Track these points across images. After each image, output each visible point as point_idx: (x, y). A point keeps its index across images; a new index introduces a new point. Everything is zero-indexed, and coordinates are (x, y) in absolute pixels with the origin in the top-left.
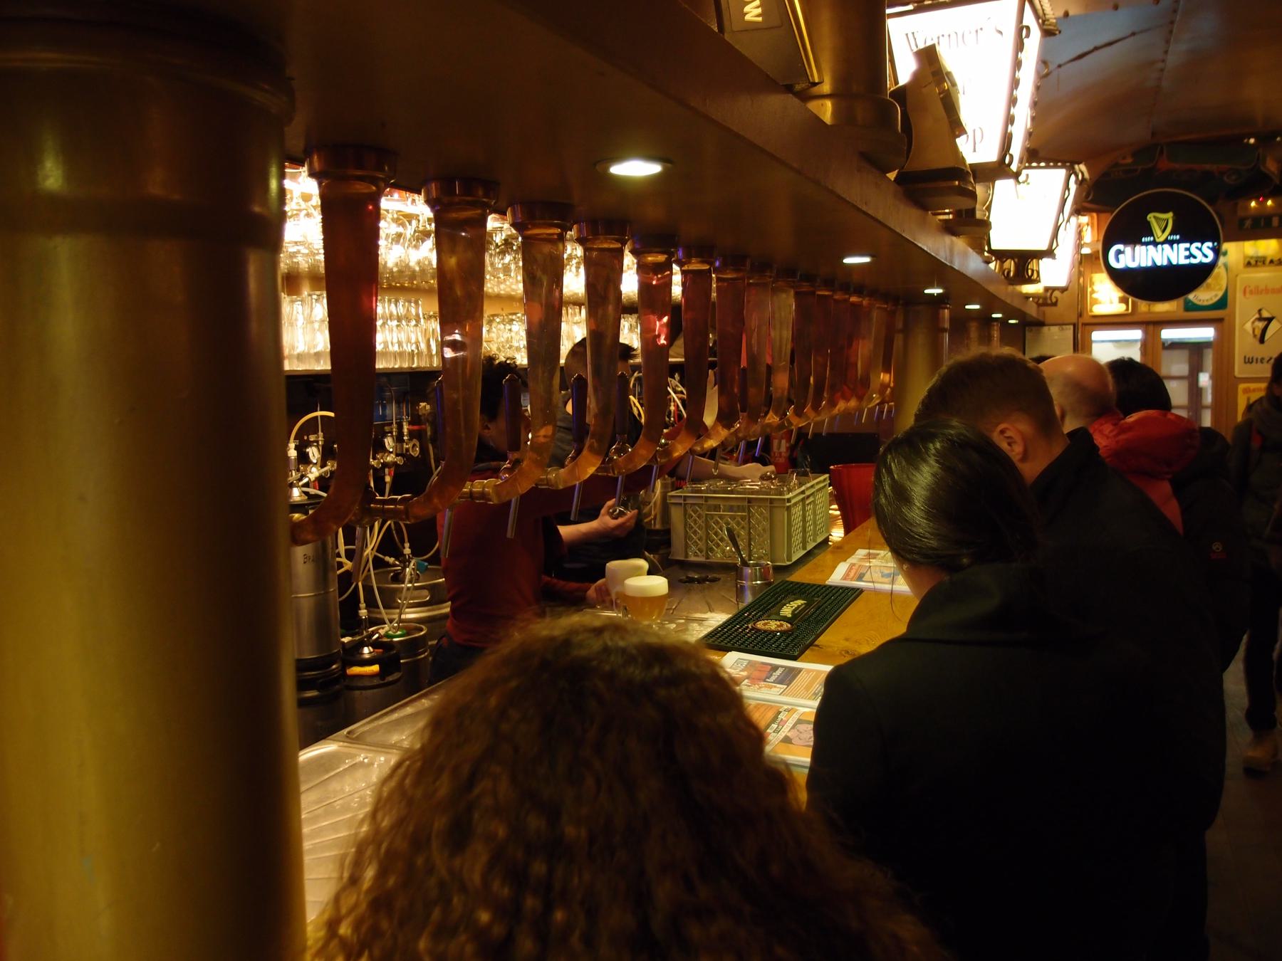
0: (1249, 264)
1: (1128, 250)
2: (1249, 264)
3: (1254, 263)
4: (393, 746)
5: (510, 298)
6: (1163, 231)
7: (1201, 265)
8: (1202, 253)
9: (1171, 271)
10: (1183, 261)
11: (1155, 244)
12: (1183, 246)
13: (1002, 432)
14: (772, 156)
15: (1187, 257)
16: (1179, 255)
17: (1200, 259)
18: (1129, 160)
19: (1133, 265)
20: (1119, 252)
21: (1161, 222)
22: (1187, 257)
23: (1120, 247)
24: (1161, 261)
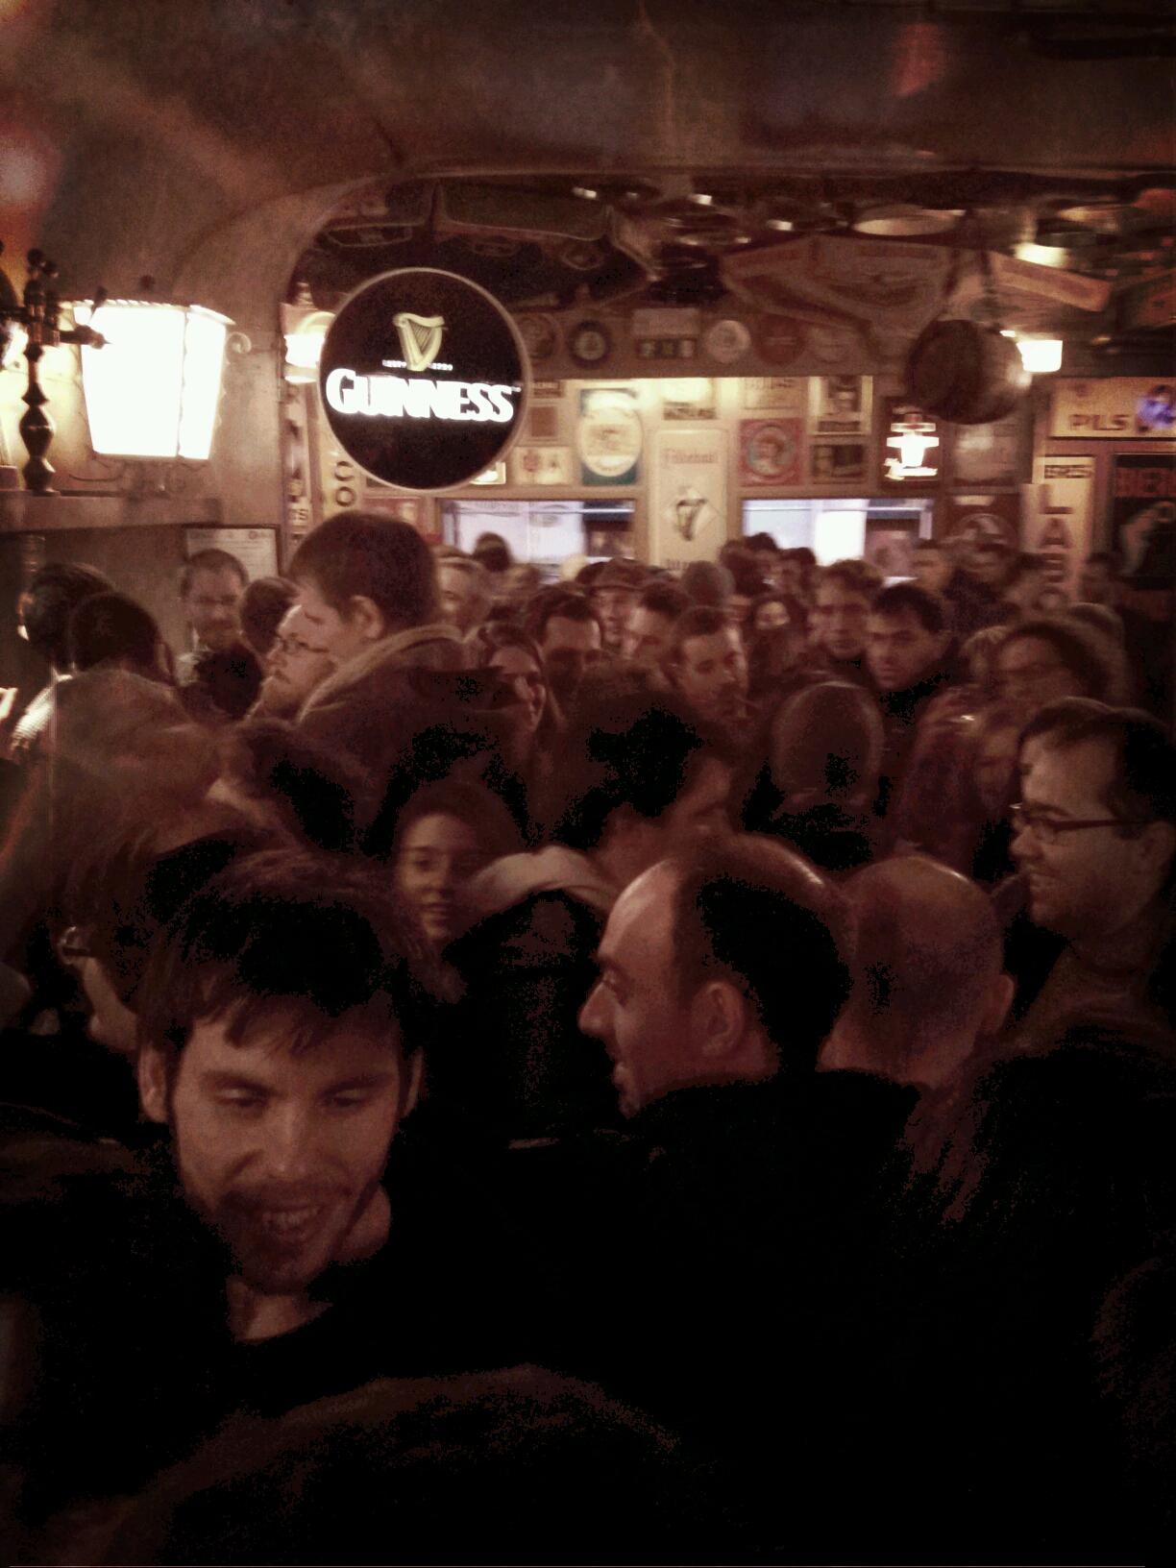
0: (669, 415)
1: (360, 381)
2: (669, 415)
3: (677, 412)
4: (555, 495)
5: (188, 573)
6: (423, 350)
7: (490, 424)
8: (491, 402)
9: (435, 428)
10: (458, 416)
11: (405, 374)
12: (455, 386)
13: (592, 260)
14: (201, 526)
15: (464, 408)
16: (444, 401)
17: (485, 415)
18: (380, 210)
19: (371, 411)
20: (347, 384)
21: (421, 335)
22: (464, 408)
23: (350, 374)
24: (419, 412)
